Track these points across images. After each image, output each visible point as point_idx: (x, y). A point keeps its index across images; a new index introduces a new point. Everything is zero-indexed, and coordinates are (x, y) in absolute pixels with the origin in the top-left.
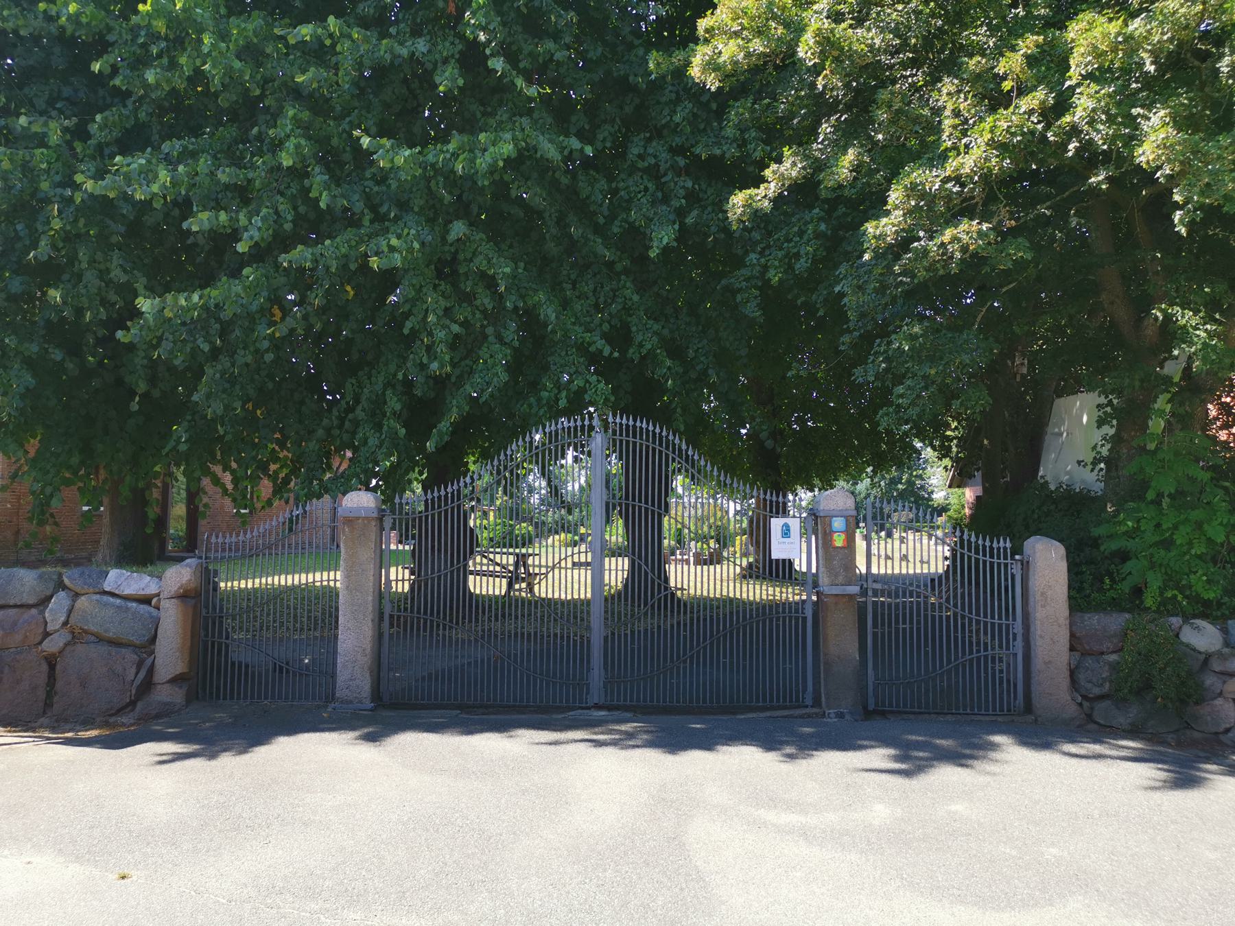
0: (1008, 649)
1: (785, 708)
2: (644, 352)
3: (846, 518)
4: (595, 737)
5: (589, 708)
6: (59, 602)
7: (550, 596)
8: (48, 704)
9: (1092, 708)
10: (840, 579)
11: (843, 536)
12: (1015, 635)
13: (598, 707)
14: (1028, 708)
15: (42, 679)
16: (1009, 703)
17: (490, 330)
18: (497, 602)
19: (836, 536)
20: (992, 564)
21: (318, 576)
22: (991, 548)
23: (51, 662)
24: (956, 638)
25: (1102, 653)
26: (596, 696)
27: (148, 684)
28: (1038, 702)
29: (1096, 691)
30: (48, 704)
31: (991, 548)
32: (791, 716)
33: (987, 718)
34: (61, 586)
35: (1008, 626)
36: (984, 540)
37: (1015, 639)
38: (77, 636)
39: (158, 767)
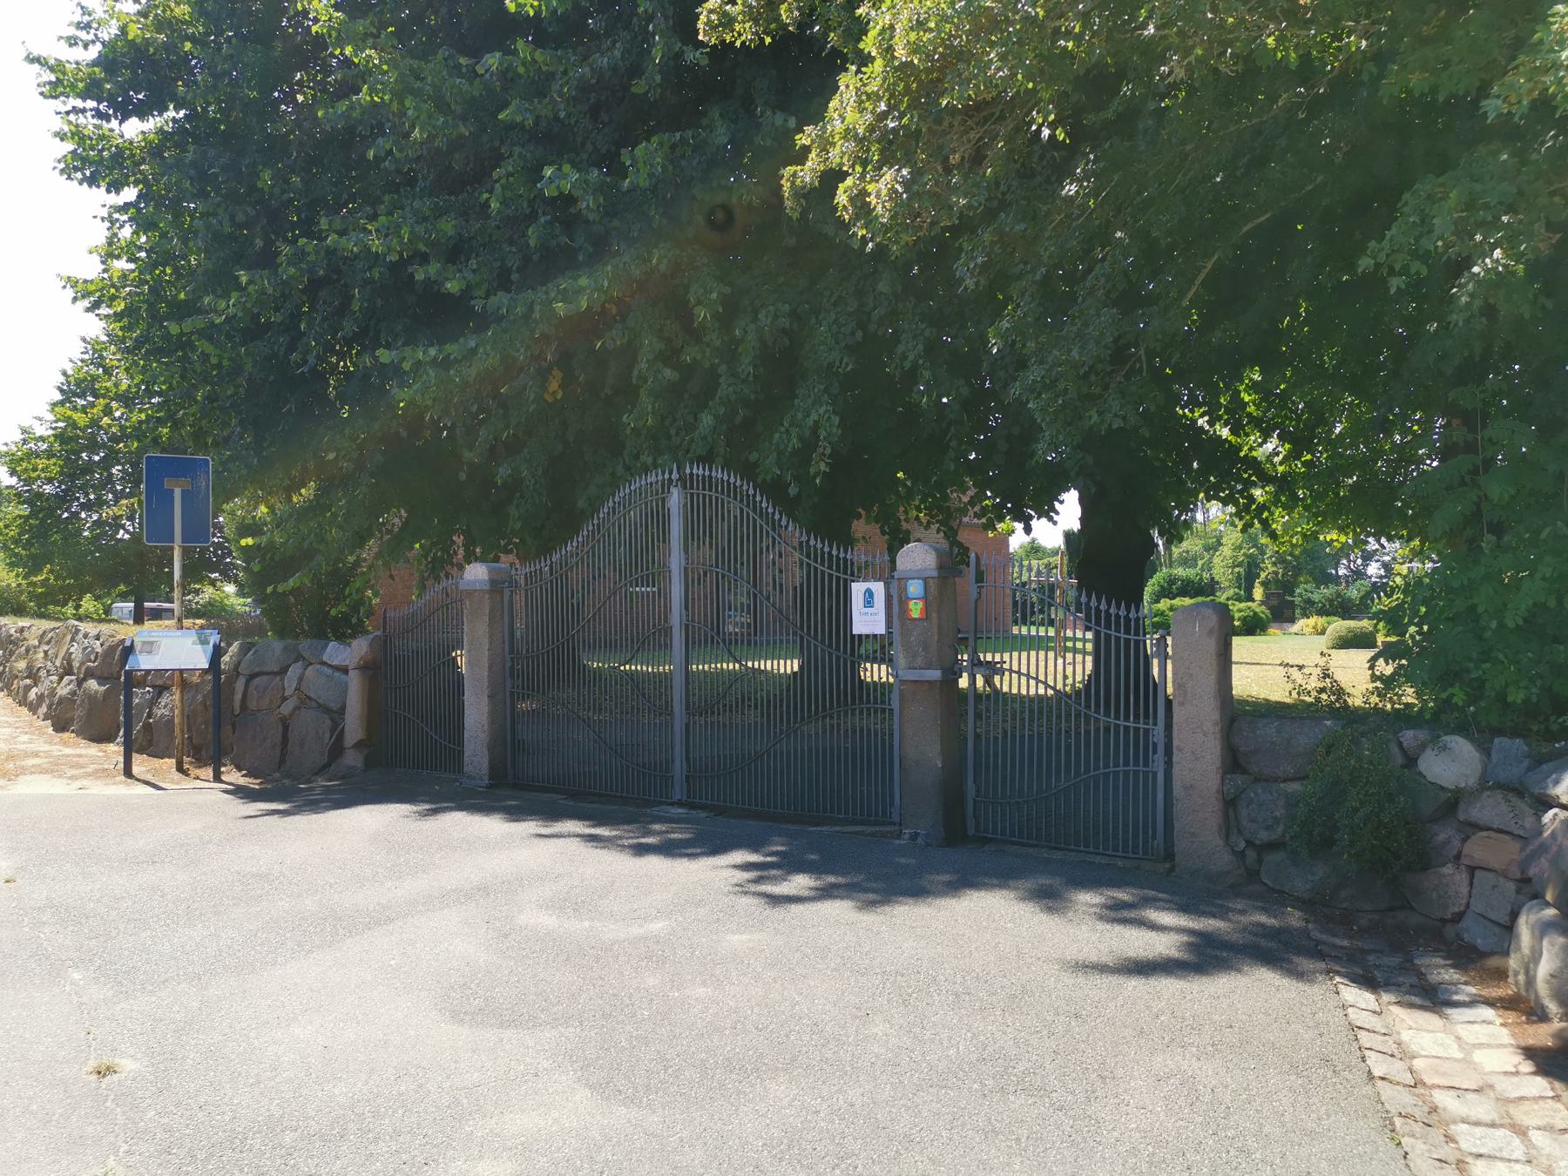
0: (1146, 764)
1: (875, 824)
2: (907, 365)
3: (925, 580)
4: (593, 831)
5: (672, 804)
6: (294, 671)
7: (1015, 691)
8: (282, 761)
9: (1260, 861)
10: (919, 661)
11: (921, 605)
12: (1155, 745)
13: (680, 804)
14: (1170, 856)
15: (278, 739)
16: (1145, 842)
17: (723, 369)
18: (875, 690)
19: (912, 605)
20: (1127, 641)
21: (1006, 657)
22: (1127, 619)
23: (285, 723)
24: (1068, 747)
25: (1276, 780)
26: (678, 793)
27: (337, 749)
28: (1180, 845)
29: (1263, 836)
30: (282, 761)
31: (1127, 619)
32: (862, 833)
33: (1098, 859)
34: (299, 658)
35: (1147, 731)
36: (1118, 608)
37: (1155, 752)
38: (305, 701)
39: (537, 840)
